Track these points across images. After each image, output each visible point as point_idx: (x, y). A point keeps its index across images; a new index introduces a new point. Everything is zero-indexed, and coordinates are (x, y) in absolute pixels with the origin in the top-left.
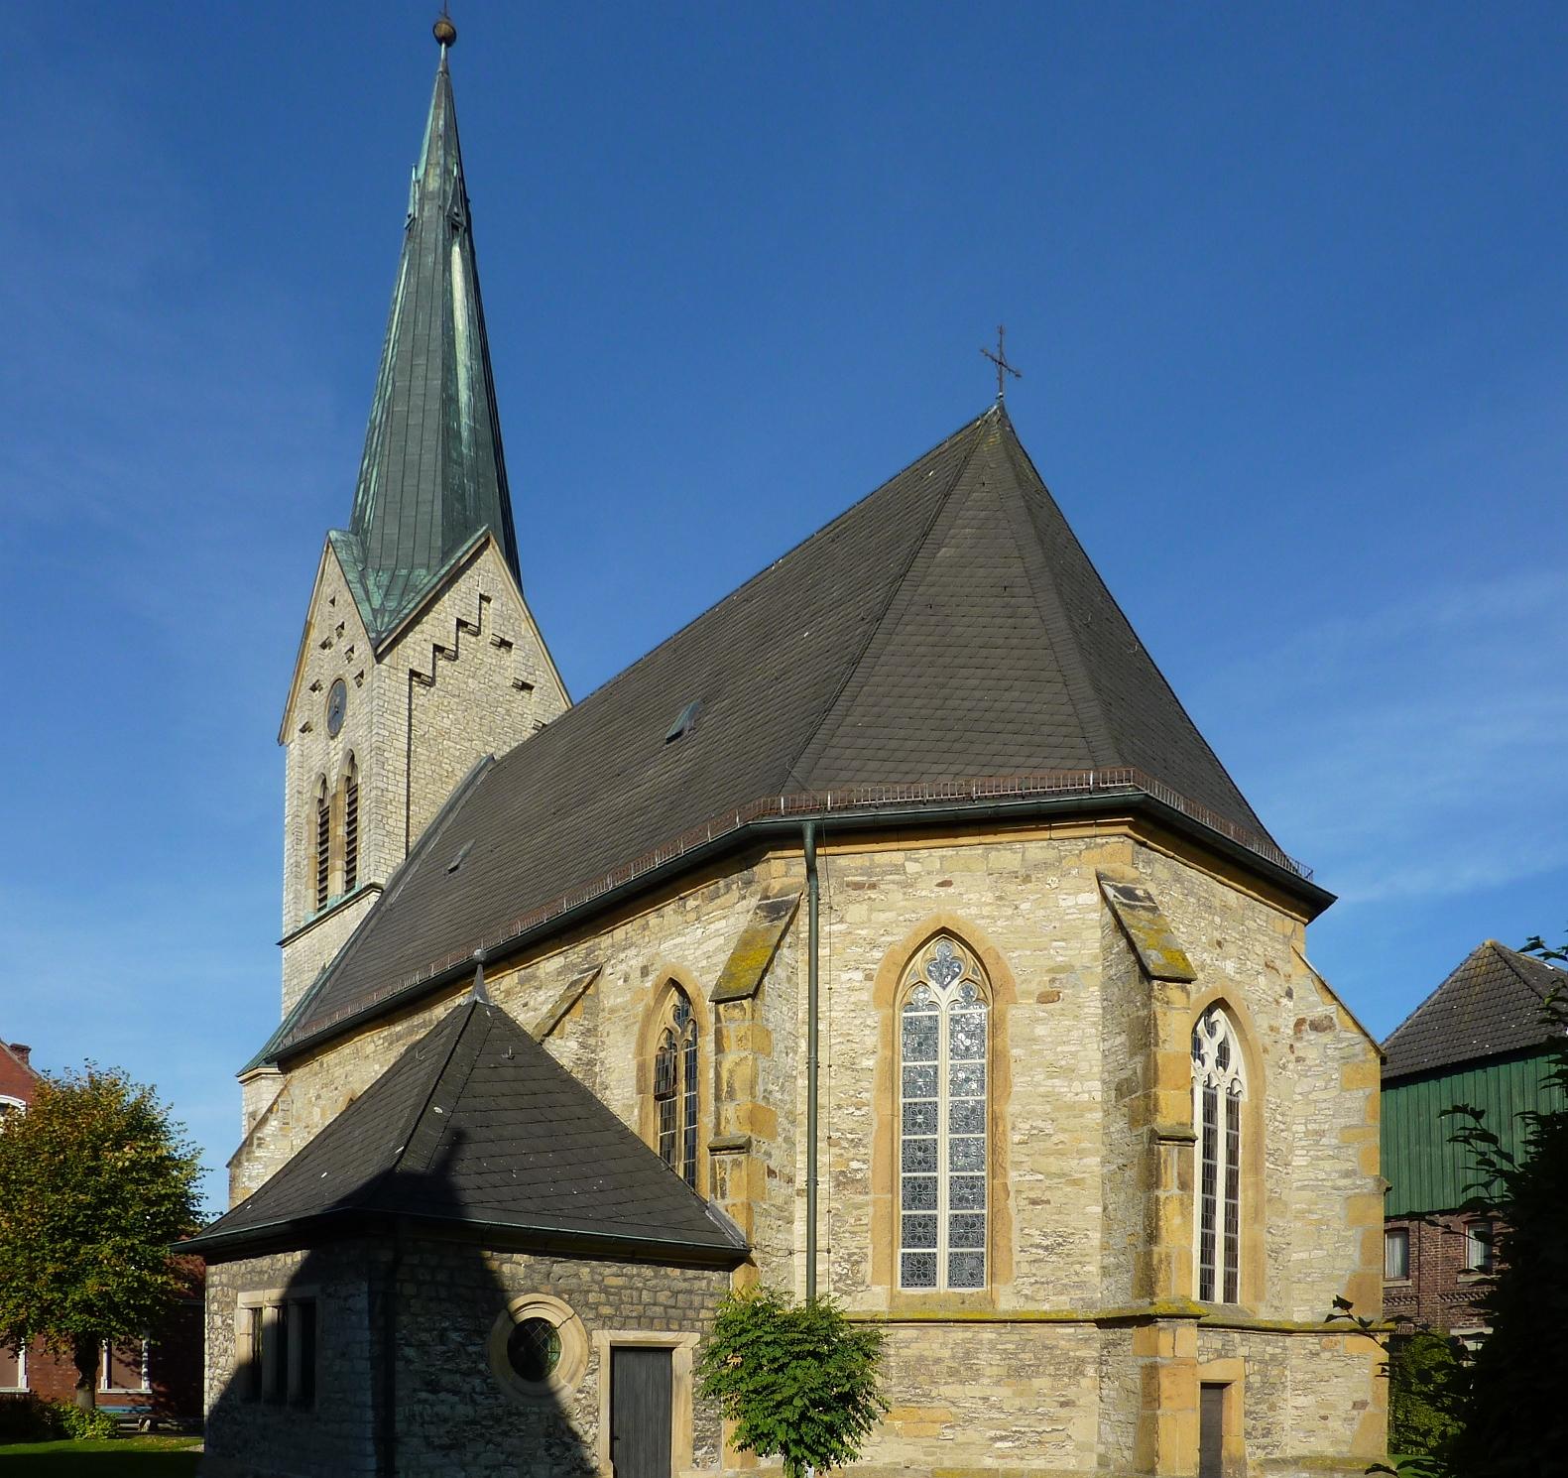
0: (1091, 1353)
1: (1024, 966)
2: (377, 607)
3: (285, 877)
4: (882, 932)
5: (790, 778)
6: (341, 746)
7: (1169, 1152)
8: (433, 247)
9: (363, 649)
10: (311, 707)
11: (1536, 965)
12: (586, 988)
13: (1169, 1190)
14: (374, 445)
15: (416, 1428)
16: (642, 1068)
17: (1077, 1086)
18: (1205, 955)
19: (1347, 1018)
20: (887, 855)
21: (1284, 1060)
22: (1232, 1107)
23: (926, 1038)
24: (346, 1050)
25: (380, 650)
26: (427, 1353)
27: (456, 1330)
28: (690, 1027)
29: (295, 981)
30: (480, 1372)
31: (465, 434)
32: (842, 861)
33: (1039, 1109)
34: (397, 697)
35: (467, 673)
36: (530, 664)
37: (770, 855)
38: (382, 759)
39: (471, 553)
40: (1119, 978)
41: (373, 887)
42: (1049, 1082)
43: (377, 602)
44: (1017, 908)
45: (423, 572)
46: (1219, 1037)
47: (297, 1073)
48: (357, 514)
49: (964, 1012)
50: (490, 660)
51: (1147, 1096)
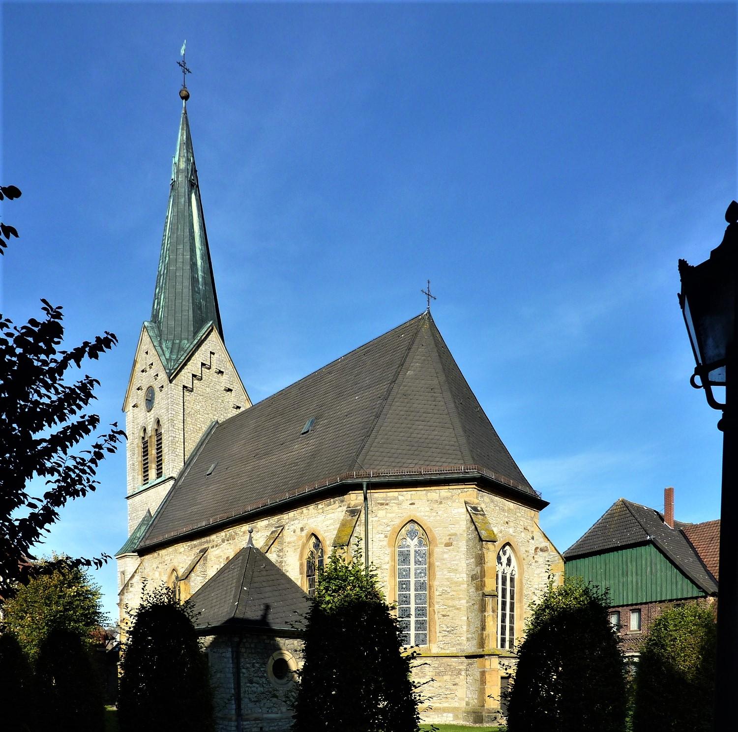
0: (463, 667)
1: (440, 533)
2: (168, 358)
3: (127, 469)
4: (390, 521)
5: (357, 463)
6: (153, 415)
7: (489, 601)
8: (183, 194)
9: (163, 376)
10: (139, 397)
11: (640, 508)
12: (279, 534)
13: (489, 613)
14: (161, 283)
15: (246, 696)
16: (301, 565)
17: (458, 576)
18: (502, 527)
19: (553, 547)
20: (392, 493)
21: (531, 562)
22: (512, 580)
23: (406, 558)
24: (170, 549)
25: (171, 378)
26: (249, 671)
27: (257, 663)
28: (320, 551)
29: (135, 514)
30: (265, 677)
31: (200, 280)
32: (376, 495)
33: (445, 583)
34: (178, 397)
35: (206, 385)
36: (231, 380)
37: (350, 492)
38: (173, 424)
39: (206, 334)
40: (472, 539)
41: (171, 478)
42: (449, 574)
43: (168, 356)
44: (437, 513)
45: (186, 342)
46: (507, 556)
47: (147, 557)
48: (154, 313)
49: (419, 549)
50: (215, 380)
51: (481, 581)
